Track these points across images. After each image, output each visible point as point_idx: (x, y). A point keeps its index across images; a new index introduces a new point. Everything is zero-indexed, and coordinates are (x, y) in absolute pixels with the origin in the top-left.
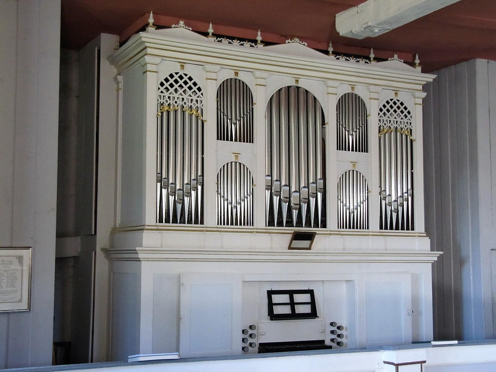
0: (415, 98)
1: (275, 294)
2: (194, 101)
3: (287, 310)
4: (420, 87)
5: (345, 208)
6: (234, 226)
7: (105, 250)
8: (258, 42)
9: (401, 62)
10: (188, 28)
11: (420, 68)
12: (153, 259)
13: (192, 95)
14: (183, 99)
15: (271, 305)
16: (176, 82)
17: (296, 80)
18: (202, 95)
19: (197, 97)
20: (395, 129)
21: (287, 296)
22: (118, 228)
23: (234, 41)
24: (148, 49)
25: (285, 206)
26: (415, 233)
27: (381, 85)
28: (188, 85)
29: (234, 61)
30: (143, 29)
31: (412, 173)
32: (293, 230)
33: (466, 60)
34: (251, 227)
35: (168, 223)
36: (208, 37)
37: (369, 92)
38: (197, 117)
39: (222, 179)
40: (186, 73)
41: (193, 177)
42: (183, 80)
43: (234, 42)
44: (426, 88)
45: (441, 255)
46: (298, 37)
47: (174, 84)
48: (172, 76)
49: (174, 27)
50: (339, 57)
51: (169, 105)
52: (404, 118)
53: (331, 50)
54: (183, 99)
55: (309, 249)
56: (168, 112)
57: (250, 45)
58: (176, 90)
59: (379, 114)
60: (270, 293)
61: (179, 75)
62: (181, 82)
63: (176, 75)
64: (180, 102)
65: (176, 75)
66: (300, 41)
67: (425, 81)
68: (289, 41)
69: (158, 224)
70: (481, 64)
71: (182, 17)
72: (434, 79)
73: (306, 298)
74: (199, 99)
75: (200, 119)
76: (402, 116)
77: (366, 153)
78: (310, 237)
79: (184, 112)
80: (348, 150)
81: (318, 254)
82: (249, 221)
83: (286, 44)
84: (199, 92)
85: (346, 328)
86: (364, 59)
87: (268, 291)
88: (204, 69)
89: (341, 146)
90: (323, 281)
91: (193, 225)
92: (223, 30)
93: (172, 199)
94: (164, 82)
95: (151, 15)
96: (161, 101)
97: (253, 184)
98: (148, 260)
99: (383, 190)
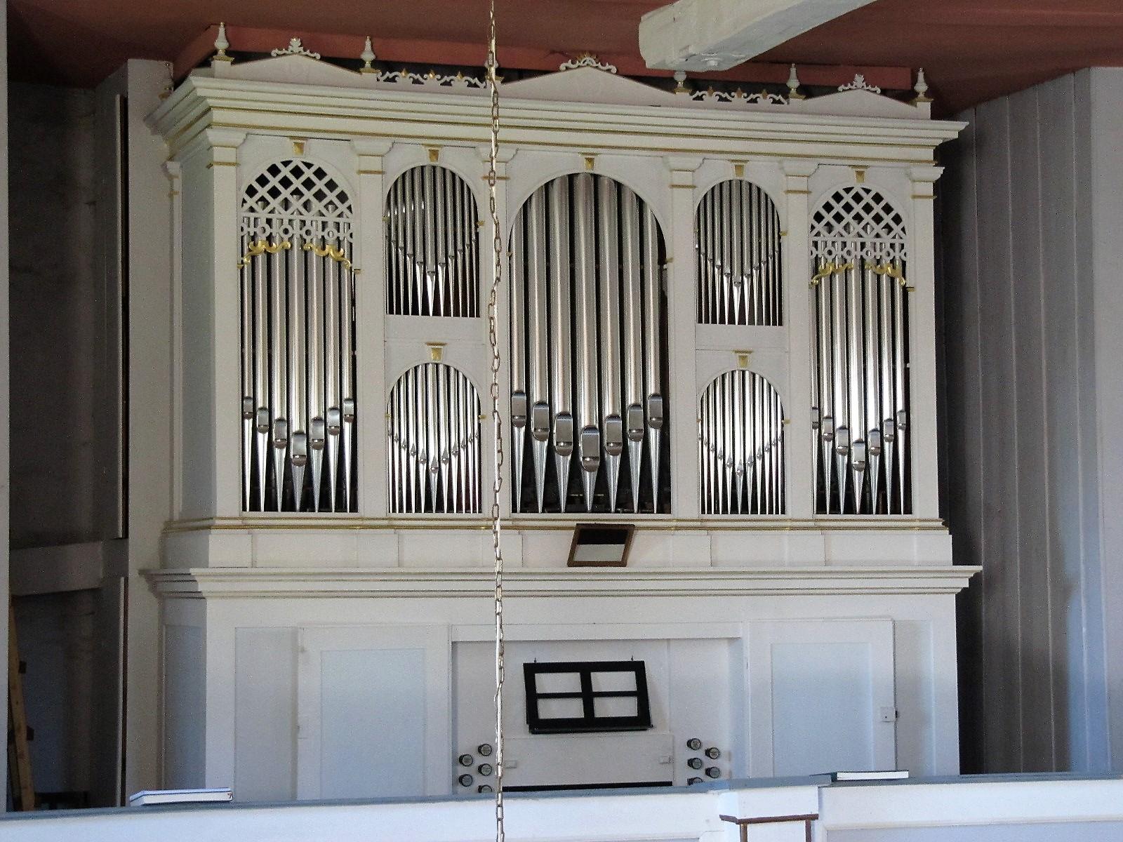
1: (599, 671)
2: (331, 227)
4: (929, 154)
5: (720, 463)
6: (434, 515)
8: (920, 96)
9: (315, 58)
10: (312, 55)
11: (928, 105)
12: (403, 594)
13: (324, 211)
14: (844, 244)
15: (532, 697)
16: (848, 208)
17: (587, 159)
18: (905, 233)
19: (270, 213)
20: (859, 263)
22: (175, 522)
23: (425, 76)
26: (914, 521)
27: (816, 156)
28: (314, 190)
29: (736, 141)
31: (907, 373)
32: (574, 520)
33: (1074, 71)
34: (477, 515)
35: (870, 514)
36: (360, 72)
37: (783, 176)
39: (710, 409)
40: (310, 162)
41: (331, 404)
42: (303, 178)
43: (426, 79)
45: (977, 575)
46: (591, 53)
47: (280, 188)
48: (274, 170)
49: (278, 55)
50: (757, 95)
51: (270, 239)
54: (844, 244)
55: (622, 563)
56: (269, 256)
57: (467, 83)
58: (286, 204)
59: (813, 228)
60: (531, 670)
61: (291, 167)
62: (297, 183)
63: (848, 193)
65: (848, 193)
66: (597, 63)
67: (940, 138)
68: (569, 64)
69: (248, 513)
72: (967, 127)
73: (626, 681)
74: (897, 242)
75: (345, 266)
76: (878, 228)
77: (778, 327)
78: (621, 535)
79: (306, 253)
80: (404, 312)
82: (469, 501)
83: (839, 94)
84: (898, 224)
85: (730, 754)
86: (768, 93)
87: (525, 665)
88: (353, 148)
89: (709, 311)
90: (668, 640)
91: (333, 514)
92: (402, 50)
94: (256, 186)
95: (222, 30)
96: (249, 230)
97: (479, 413)
98: (223, 596)
99: (826, 414)
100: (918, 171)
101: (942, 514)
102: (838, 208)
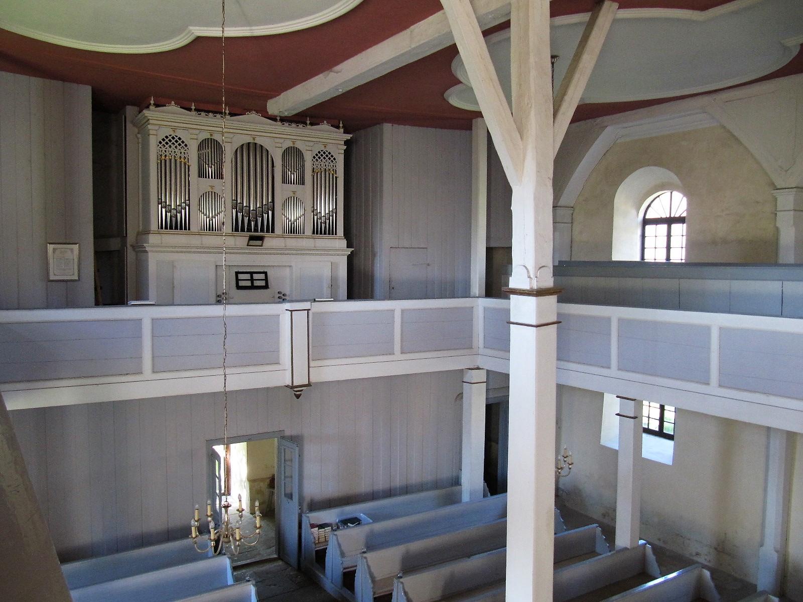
0: (339, 149)
2: (183, 153)
3: (249, 284)
5: (288, 220)
7: (132, 246)
11: (343, 130)
15: (237, 280)
16: (322, 155)
21: (249, 275)
24: (150, 121)
25: (246, 220)
30: (148, 107)
38: (185, 164)
44: (347, 143)
45: (353, 251)
47: (169, 142)
48: (167, 137)
52: (331, 162)
53: (193, 107)
55: (262, 246)
56: (165, 161)
60: (237, 273)
61: (171, 136)
62: (173, 141)
64: (173, 154)
70: (387, 127)
71: (173, 99)
73: (262, 276)
78: (261, 238)
81: (266, 249)
89: (202, 174)
92: (202, 106)
93: (169, 214)
98: (153, 251)
100: (339, 146)
101: (344, 235)
102: (319, 155)
